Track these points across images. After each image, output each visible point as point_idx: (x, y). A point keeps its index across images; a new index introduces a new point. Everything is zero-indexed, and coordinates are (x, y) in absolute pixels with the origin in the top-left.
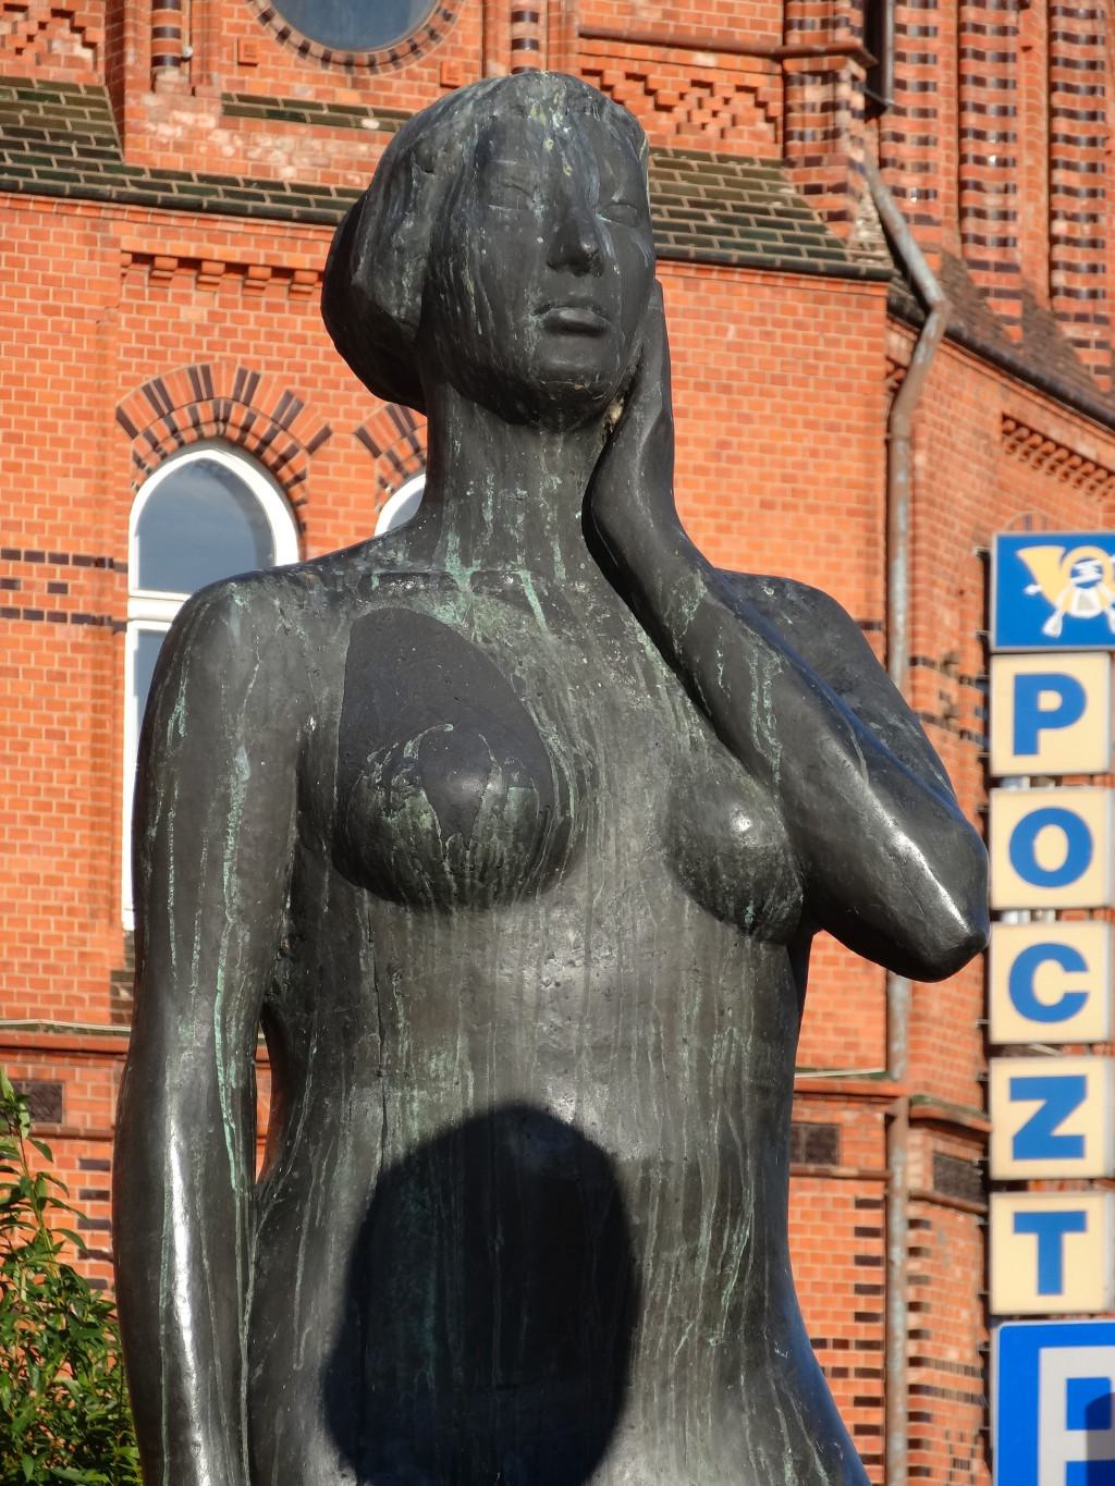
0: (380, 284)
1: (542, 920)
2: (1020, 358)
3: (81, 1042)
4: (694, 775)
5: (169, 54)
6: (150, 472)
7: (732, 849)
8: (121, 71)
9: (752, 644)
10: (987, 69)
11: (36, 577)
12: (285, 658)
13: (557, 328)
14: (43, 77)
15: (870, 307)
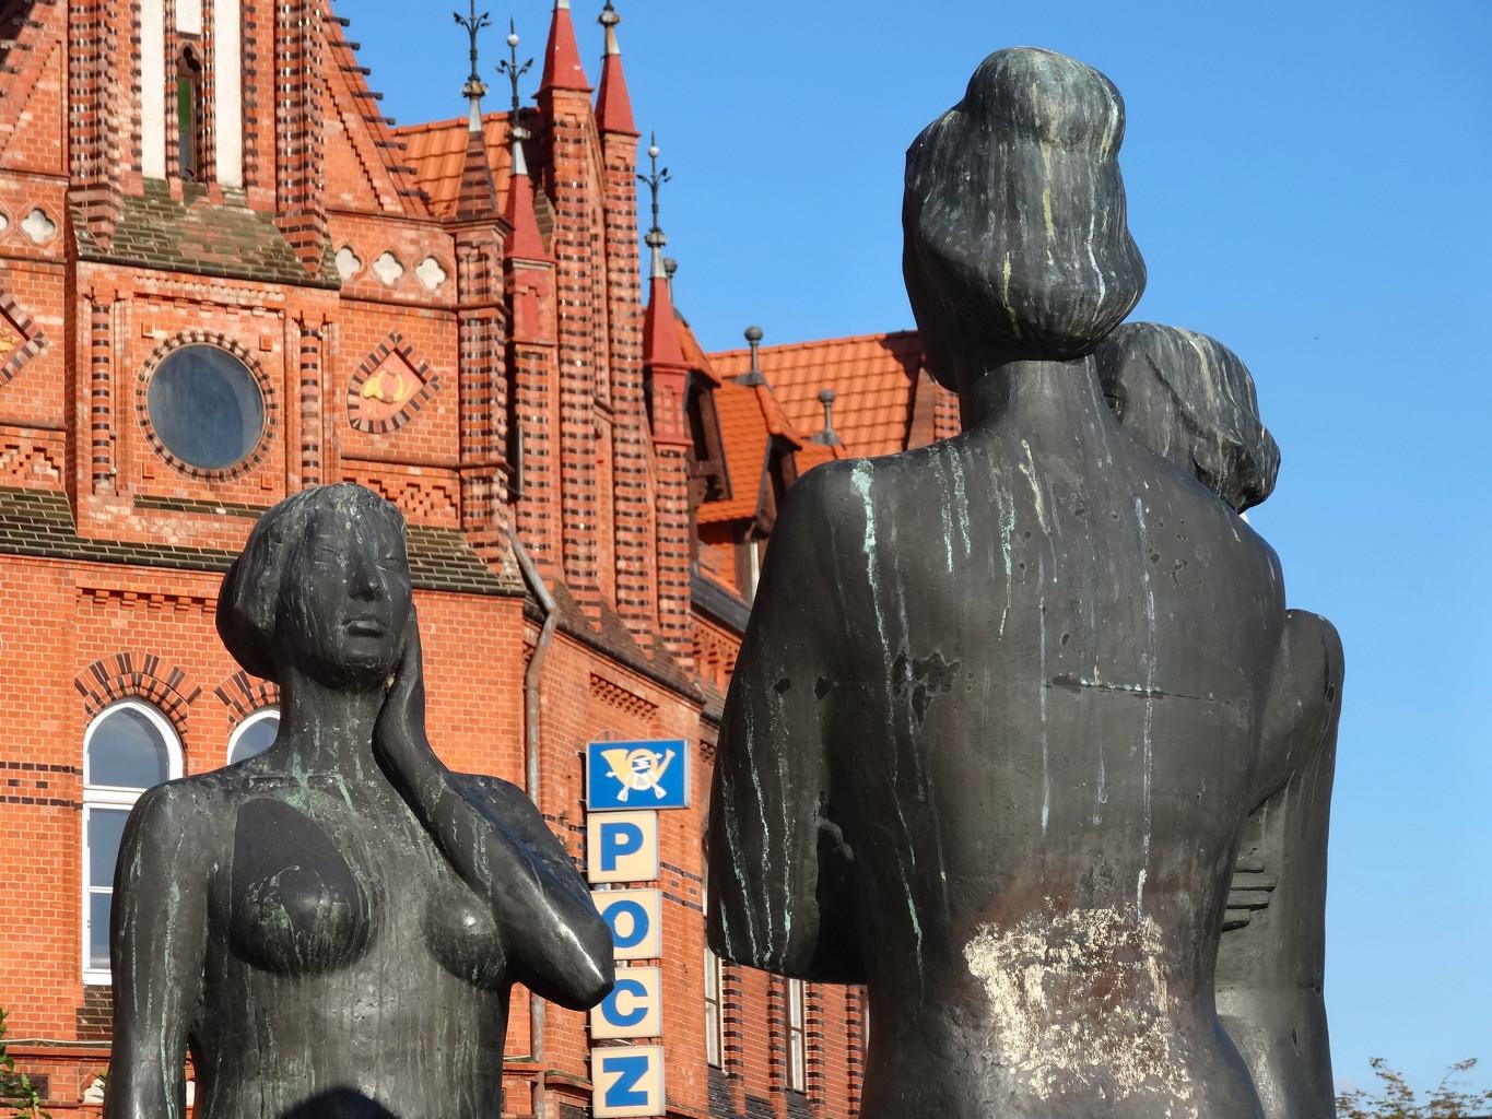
0: (251, 608)
1: (354, 980)
2: (601, 641)
3: (58, 1051)
4: (441, 893)
5: (103, 473)
6: (95, 716)
7: (464, 936)
8: (75, 482)
9: (474, 816)
10: (578, 474)
11: (29, 779)
12: (199, 829)
13: (355, 632)
14: (29, 487)
15: (513, 612)
